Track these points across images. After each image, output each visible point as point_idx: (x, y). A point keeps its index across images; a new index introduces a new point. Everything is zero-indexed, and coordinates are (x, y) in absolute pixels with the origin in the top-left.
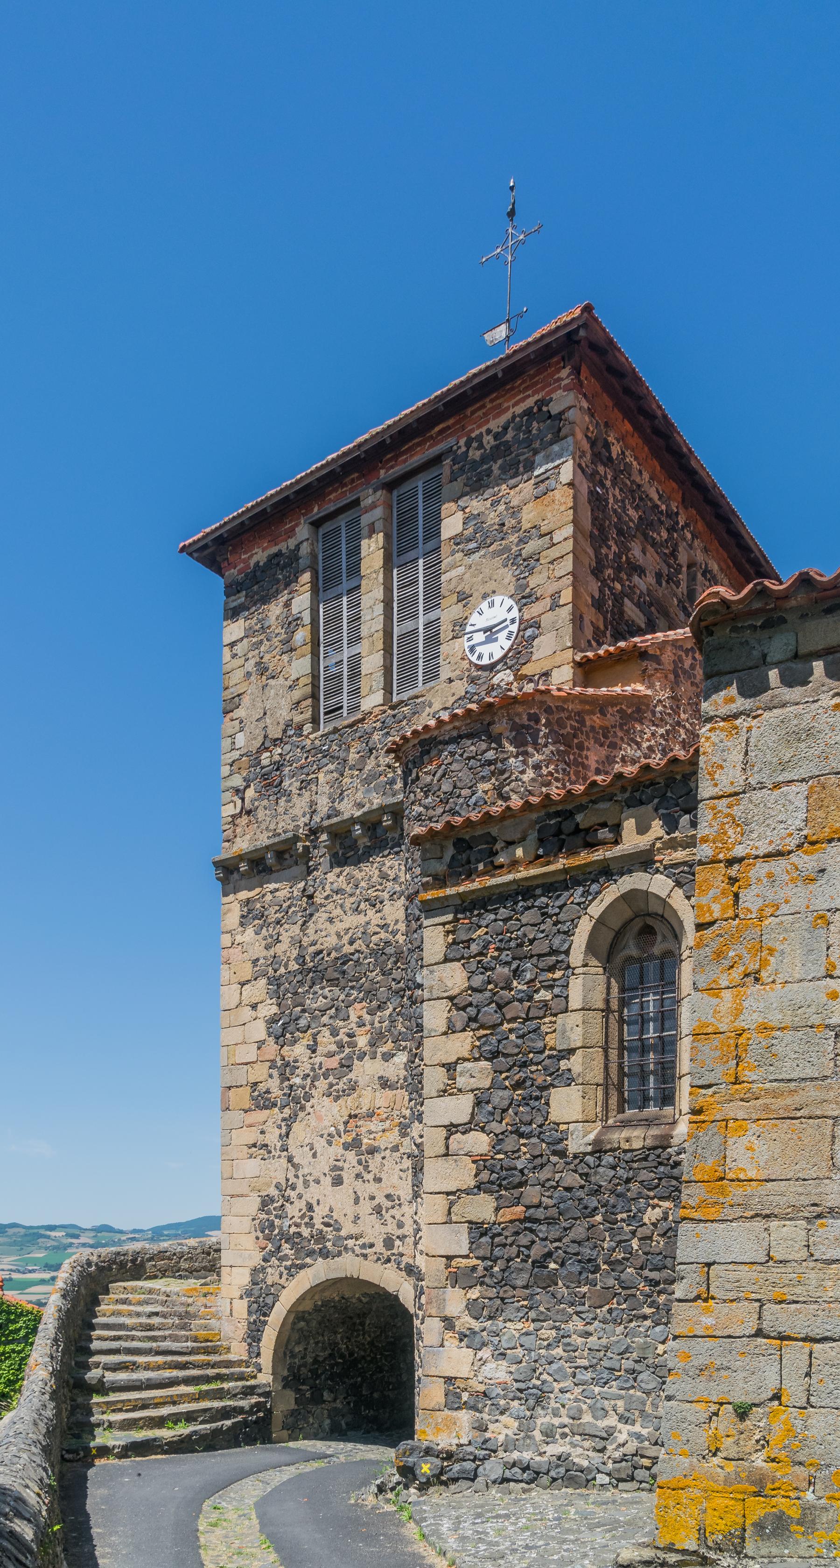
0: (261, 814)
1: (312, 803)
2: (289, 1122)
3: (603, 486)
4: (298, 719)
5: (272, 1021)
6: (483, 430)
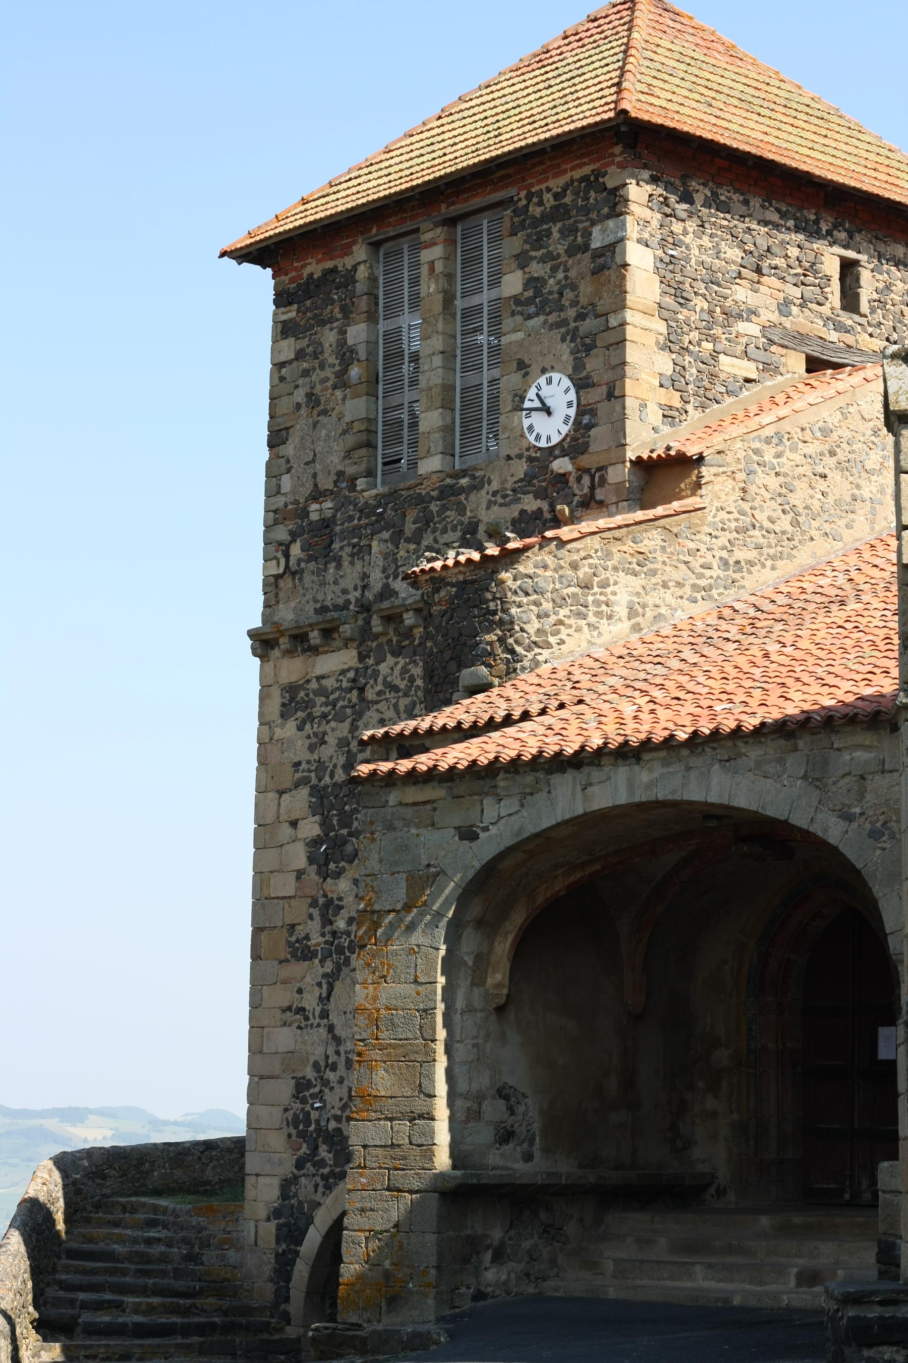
0: (307, 577)
1: (365, 576)
2: (331, 978)
4: (351, 470)
5: (315, 843)
6: (543, 186)
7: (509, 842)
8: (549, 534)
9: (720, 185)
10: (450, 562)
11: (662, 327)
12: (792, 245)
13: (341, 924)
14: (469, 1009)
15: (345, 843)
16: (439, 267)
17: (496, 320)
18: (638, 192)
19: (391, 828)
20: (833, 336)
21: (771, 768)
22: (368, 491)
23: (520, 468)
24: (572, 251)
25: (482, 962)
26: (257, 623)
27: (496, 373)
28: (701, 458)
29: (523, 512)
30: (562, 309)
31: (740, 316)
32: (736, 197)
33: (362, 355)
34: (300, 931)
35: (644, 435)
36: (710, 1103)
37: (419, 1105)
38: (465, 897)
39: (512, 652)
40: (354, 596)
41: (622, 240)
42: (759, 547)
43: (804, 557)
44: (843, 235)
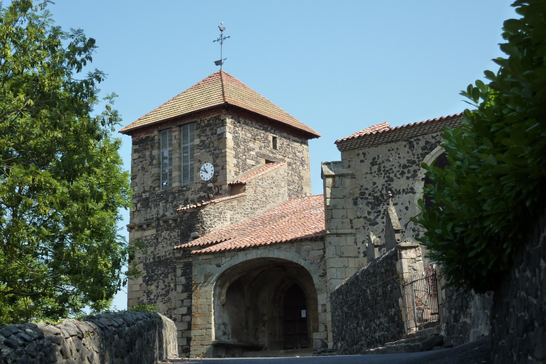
0: (142, 212)
1: (158, 211)
3: (237, 133)
4: (154, 186)
5: (145, 277)
7: (228, 267)
8: (212, 201)
9: (246, 119)
10: (188, 208)
11: (234, 153)
12: (262, 133)
13: (152, 297)
14: (218, 305)
15: (153, 277)
16: (177, 137)
17: (192, 149)
18: (229, 121)
19: (200, 264)
20: (271, 155)
21: (288, 250)
22: (158, 191)
23: (200, 186)
24: (212, 134)
25: (220, 294)
26: (128, 223)
27: (192, 163)
28: (245, 183)
29: (200, 196)
30: (210, 148)
31: (251, 150)
32: (250, 122)
33: (157, 157)
34: (141, 299)
35: (231, 178)
36: (263, 329)
37: (208, 326)
38: (217, 281)
39: (204, 229)
40: (155, 216)
41: (225, 132)
42: (259, 204)
43: (268, 207)
44: (273, 131)
